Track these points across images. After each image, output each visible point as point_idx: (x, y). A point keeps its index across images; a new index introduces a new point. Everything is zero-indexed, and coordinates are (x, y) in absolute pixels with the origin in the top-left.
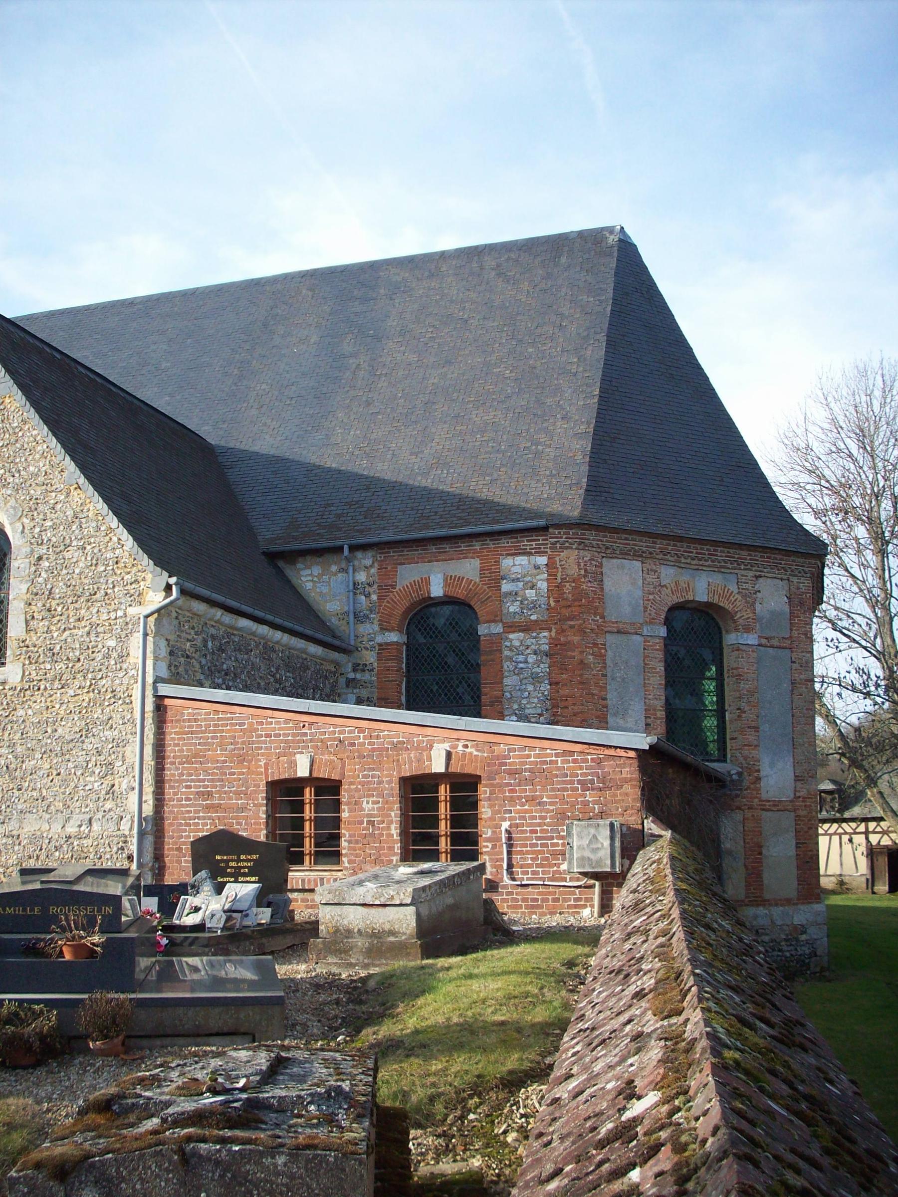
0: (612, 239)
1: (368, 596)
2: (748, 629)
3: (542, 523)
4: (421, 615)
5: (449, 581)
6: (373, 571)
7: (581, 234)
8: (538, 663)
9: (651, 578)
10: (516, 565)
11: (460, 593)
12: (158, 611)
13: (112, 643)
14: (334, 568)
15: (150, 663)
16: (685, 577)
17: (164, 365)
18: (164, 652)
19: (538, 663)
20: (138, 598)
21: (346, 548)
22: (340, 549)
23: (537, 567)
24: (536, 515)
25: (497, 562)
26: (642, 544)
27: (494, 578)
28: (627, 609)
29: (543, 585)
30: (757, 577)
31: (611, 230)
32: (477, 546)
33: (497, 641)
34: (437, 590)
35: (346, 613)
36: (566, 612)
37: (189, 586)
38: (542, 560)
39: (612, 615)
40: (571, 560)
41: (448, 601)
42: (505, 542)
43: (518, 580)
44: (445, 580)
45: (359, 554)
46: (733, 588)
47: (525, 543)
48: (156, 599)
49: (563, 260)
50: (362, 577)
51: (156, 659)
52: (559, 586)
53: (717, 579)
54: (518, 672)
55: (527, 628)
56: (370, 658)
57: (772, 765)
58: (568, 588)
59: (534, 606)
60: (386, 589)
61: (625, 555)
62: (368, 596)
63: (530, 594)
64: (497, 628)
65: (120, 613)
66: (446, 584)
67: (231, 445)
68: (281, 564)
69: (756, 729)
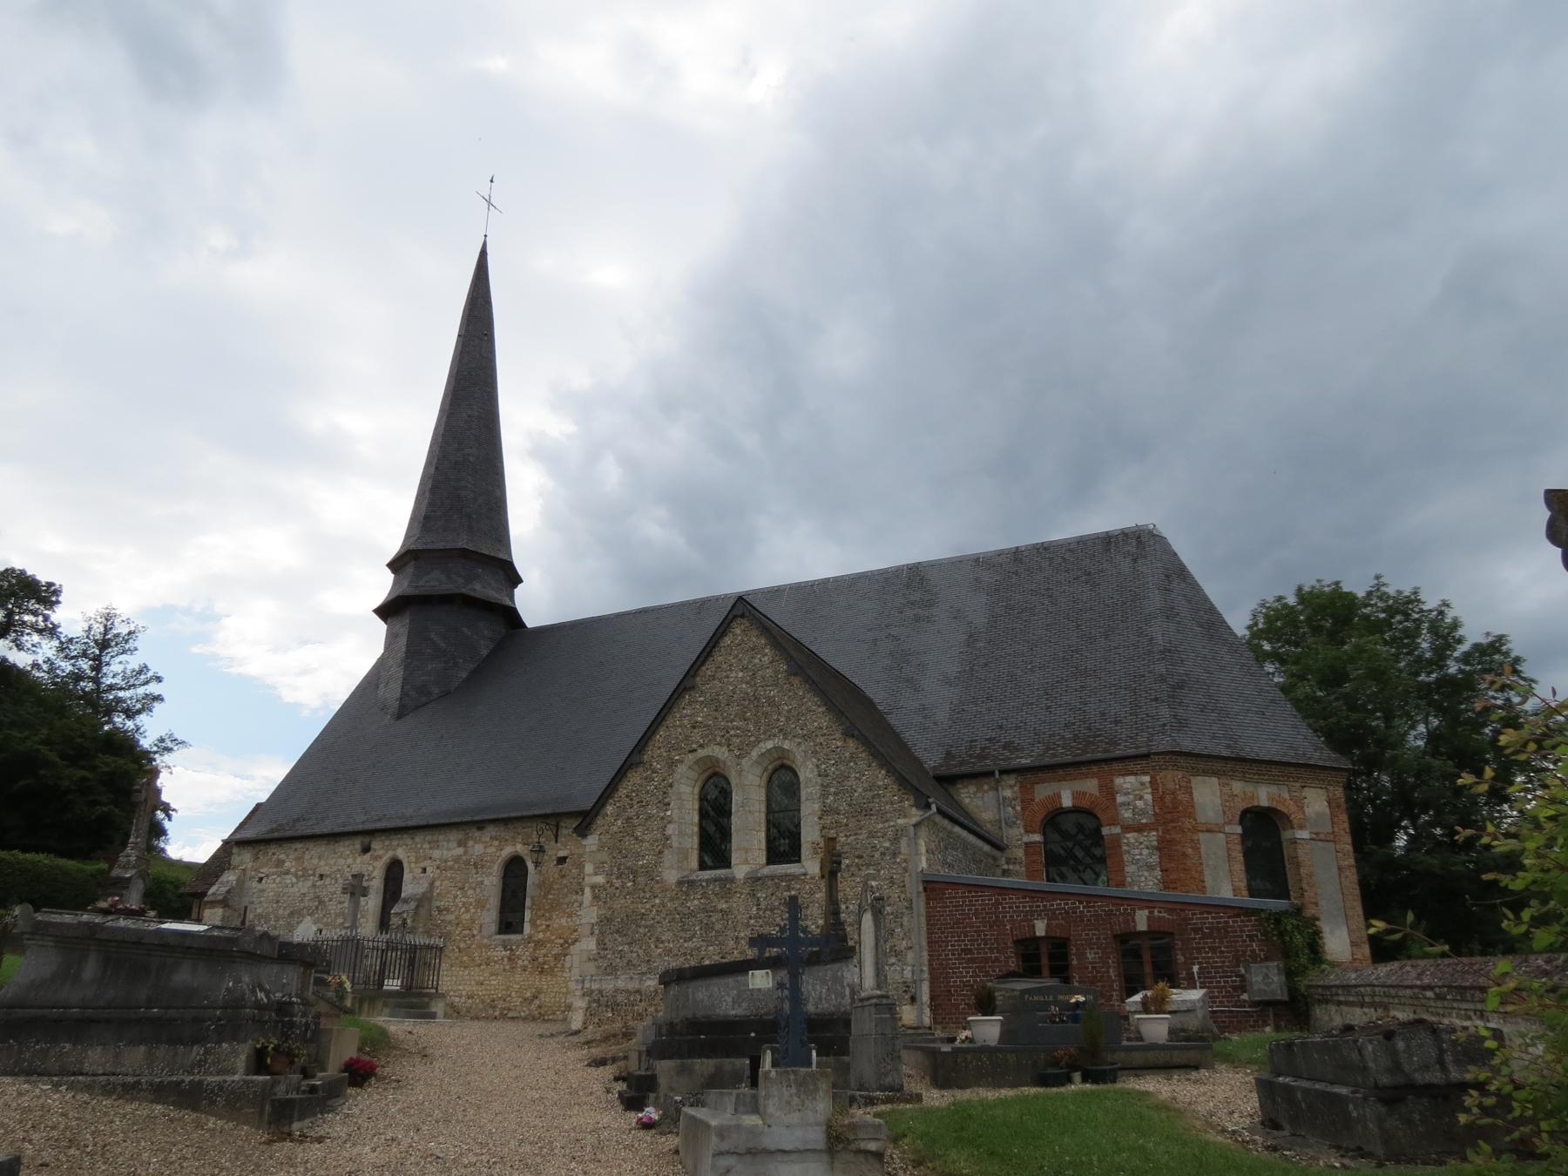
2: (1301, 827)
4: (1053, 820)
8: (1151, 855)
9: (1226, 790)
10: (1126, 782)
11: (1085, 804)
13: (887, 844)
16: (1250, 788)
19: (1151, 855)
22: (992, 773)
23: (1142, 784)
26: (1218, 765)
27: (1109, 792)
28: (1211, 814)
29: (1149, 797)
32: (1095, 769)
33: (1116, 839)
34: (1067, 802)
36: (1169, 816)
37: (944, 808)
38: (1147, 779)
39: (1201, 818)
42: (1116, 766)
46: (1286, 796)
47: (1131, 766)
50: (1008, 793)
52: (1162, 798)
53: (1274, 789)
54: (1135, 862)
55: (1140, 829)
56: (1020, 853)
57: (1332, 933)
58: (1168, 799)
59: (1143, 812)
60: (1026, 802)
61: (1206, 773)
63: (1139, 804)
64: (1117, 830)
69: (1316, 904)
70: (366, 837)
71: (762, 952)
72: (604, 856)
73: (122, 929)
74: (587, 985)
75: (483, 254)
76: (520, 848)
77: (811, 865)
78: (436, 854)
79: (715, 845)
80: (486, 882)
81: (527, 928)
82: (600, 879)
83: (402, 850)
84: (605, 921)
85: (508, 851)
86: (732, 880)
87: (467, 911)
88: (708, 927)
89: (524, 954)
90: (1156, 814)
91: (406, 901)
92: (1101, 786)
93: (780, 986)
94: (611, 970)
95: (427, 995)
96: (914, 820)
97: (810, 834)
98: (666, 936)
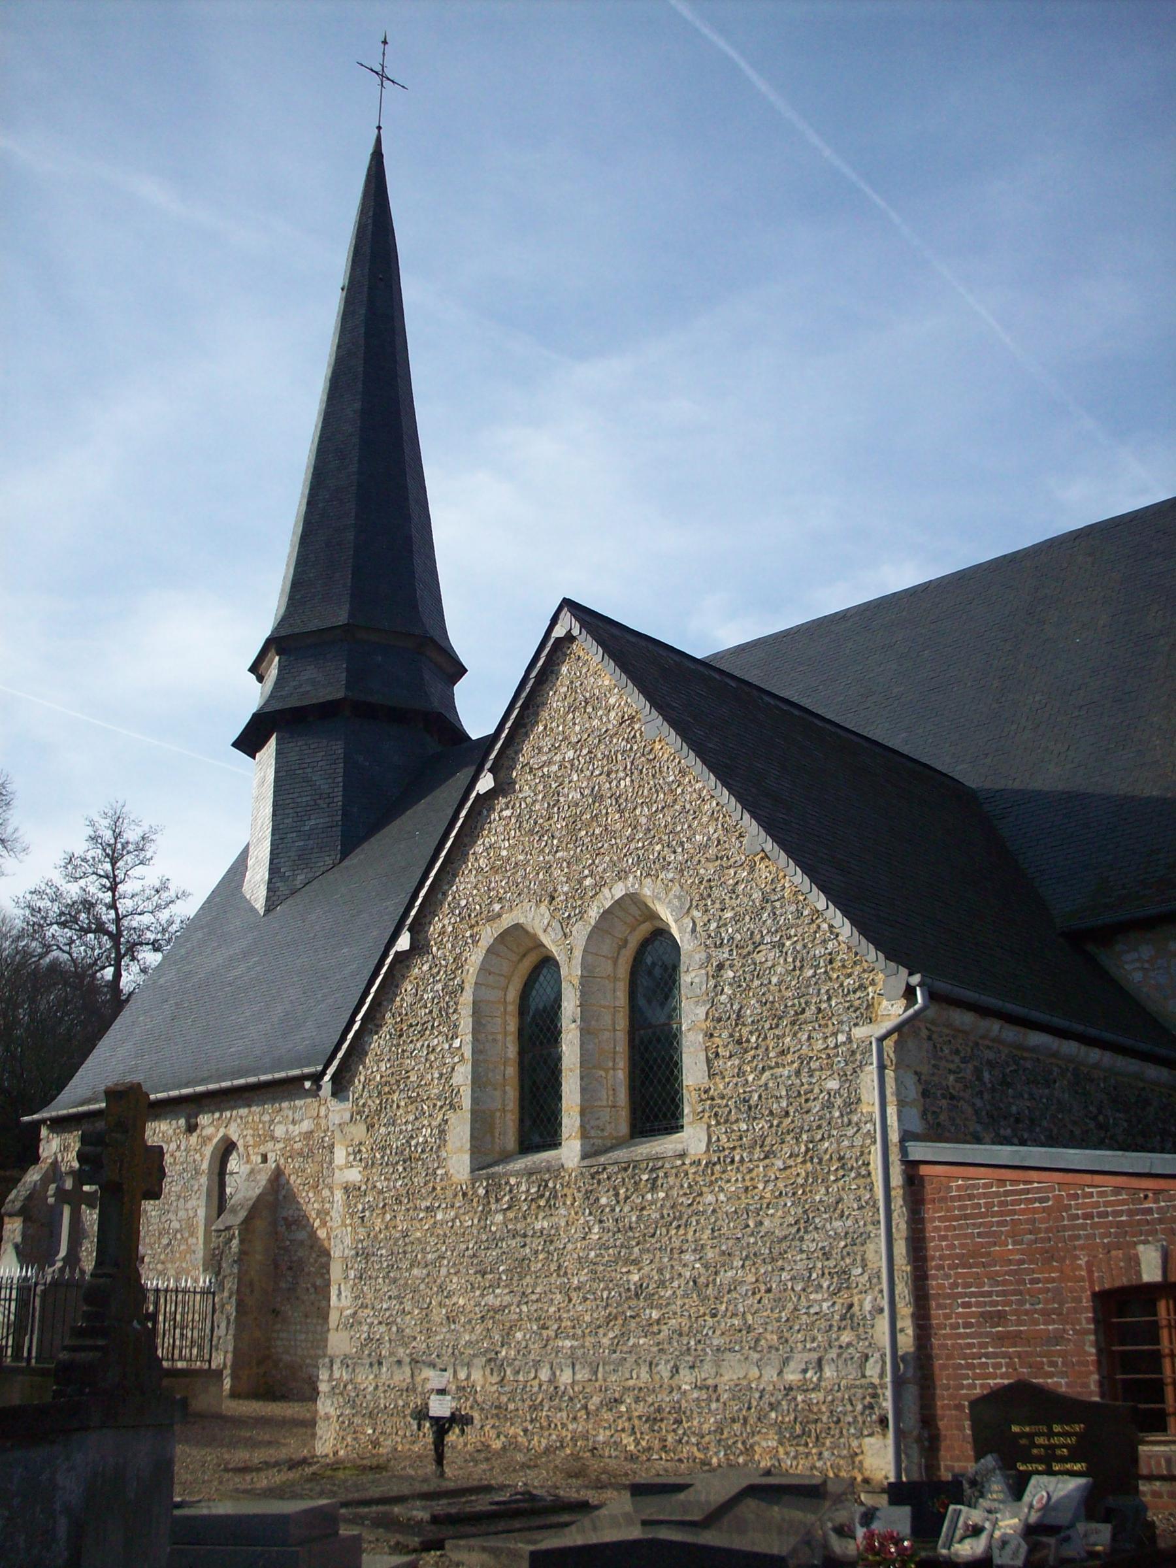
12: (898, 1029)
13: (833, 1085)
15: (892, 1110)
18: (913, 1092)
20: (867, 1013)
37: (942, 986)
48: (893, 1011)
51: (901, 1104)
65: (842, 1038)
68: (1091, 948)
72: (358, 1131)
75: (377, 157)
86: (557, 1171)
96: (887, 1025)
98: (454, 1283)
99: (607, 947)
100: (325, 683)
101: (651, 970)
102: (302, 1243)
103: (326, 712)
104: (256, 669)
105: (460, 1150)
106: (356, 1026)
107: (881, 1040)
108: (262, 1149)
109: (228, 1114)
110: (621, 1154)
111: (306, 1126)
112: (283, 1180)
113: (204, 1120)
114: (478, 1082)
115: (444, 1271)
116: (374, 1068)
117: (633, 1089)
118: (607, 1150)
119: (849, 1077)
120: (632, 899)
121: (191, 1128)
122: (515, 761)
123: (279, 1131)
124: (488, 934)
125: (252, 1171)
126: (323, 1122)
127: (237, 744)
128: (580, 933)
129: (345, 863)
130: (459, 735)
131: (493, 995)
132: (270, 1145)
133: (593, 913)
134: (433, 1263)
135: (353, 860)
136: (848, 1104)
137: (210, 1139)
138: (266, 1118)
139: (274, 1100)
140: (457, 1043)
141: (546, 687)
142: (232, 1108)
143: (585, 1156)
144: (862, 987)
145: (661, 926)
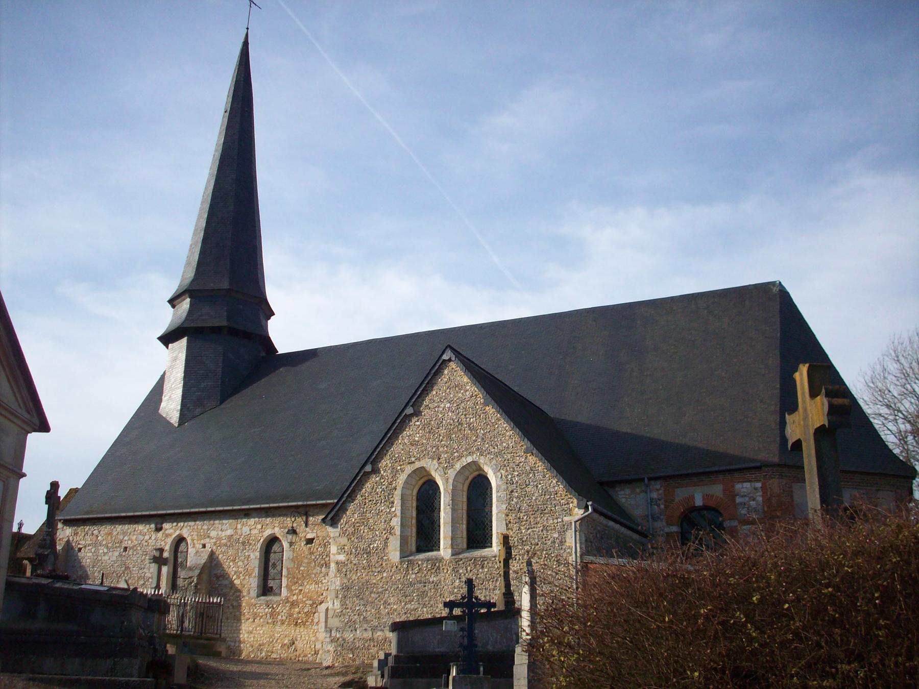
0: (775, 290)
1: (659, 506)
3: (758, 464)
5: (706, 497)
6: (661, 492)
7: (756, 286)
12: (581, 519)
13: (556, 535)
14: (638, 490)
15: (578, 545)
17: (511, 367)
18: (584, 539)
20: (570, 512)
21: (646, 479)
22: (643, 480)
23: (756, 489)
24: (753, 460)
25: (733, 486)
27: (731, 495)
29: (760, 499)
30: (878, 490)
31: (773, 283)
32: (721, 477)
34: (699, 502)
35: (647, 516)
37: (600, 508)
38: (759, 485)
40: (775, 484)
41: (705, 508)
42: (736, 475)
43: (745, 496)
44: (703, 497)
45: (653, 483)
48: (579, 513)
49: (747, 303)
50: (655, 495)
51: (581, 543)
56: (661, 539)
58: (774, 500)
59: (755, 510)
62: (659, 506)
64: (734, 523)
65: (559, 520)
66: (704, 499)
67: (563, 418)
68: (606, 488)
70: (159, 520)
71: (451, 611)
72: (344, 540)
73: (58, 588)
74: (333, 634)
75: (246, 44)
76: (277, 532)
77: (496, 547)
78: (213, 534)
79: (425, 535)
80: (252, 556)
81: (284, 592)
82: (342, 557)
83: (187, 529)
84: (346, 588)
85: (268, 532)
86: (441, 560)
87: (238, 577)
88: (423, 594)
89: (283, 611)
90: (764, 512)
91: (191, 569)
92: (724, 490)
93: (462, 629)
94: (351, 625)
95: (214, 639)
96: (577, 518)
97: (497, 528)
98: (392, 600)
99: (461, 479)
100: (216, 317)
101: (477, 489)
102: (226, 586)
103: (216, 330)
104: (173, 302)
105: (395, 550)
106: (344, 499)
107: (576, 522)
108: (202, 542)
109: (182, 524)
110: (466, 555)
111: (229, 532)
112: (215, 557)
113: (166, 526)
114: (403, 525)
115: (387, 595)
116: (352, 514)
117: (468, 531)
118: (460, 553)
119: (562, 532)
120: (474, 463)
121: (158, 529)
122: (422, 404)
123: (213, 534)
124: (409, 469)
125: (197, 552)
126: (239, 532)
127: (160, 339)
128: (452, 473)
129: (222, 406)
130: (269, 346)
131: (409, 492)
132: (207, 540)
133: (458, 466)
134: (382, 592)
135: (227, 405)
136: (561, 542)
137: (171, 535)
138: (205, 527)
139: (210, 519)
140: (393, 509)
141: (437, 377)
142: (185, 522)
143: (453, 555)
144: (568, 504)
145: (481, 472)
